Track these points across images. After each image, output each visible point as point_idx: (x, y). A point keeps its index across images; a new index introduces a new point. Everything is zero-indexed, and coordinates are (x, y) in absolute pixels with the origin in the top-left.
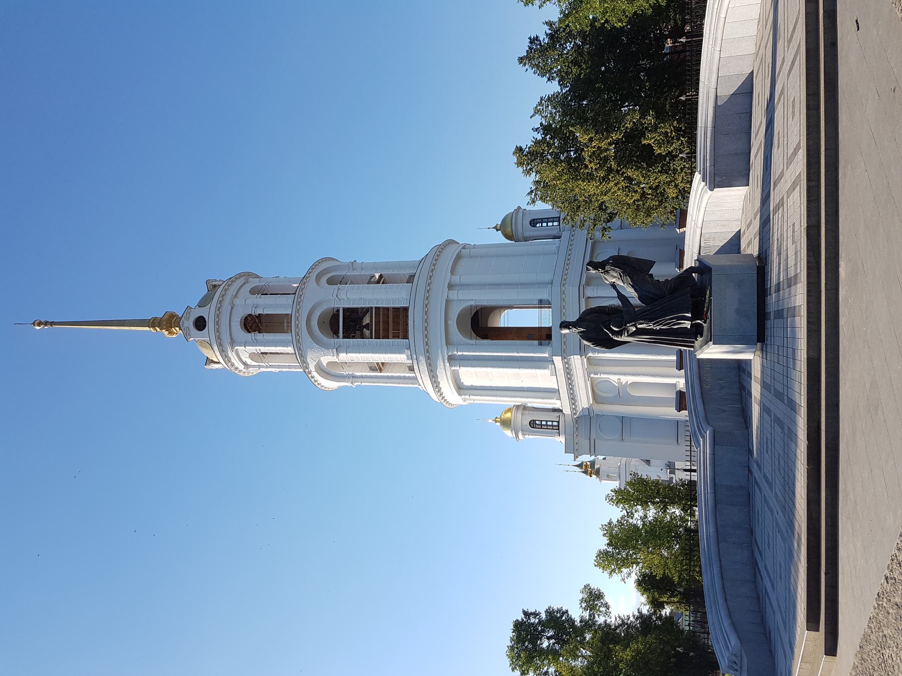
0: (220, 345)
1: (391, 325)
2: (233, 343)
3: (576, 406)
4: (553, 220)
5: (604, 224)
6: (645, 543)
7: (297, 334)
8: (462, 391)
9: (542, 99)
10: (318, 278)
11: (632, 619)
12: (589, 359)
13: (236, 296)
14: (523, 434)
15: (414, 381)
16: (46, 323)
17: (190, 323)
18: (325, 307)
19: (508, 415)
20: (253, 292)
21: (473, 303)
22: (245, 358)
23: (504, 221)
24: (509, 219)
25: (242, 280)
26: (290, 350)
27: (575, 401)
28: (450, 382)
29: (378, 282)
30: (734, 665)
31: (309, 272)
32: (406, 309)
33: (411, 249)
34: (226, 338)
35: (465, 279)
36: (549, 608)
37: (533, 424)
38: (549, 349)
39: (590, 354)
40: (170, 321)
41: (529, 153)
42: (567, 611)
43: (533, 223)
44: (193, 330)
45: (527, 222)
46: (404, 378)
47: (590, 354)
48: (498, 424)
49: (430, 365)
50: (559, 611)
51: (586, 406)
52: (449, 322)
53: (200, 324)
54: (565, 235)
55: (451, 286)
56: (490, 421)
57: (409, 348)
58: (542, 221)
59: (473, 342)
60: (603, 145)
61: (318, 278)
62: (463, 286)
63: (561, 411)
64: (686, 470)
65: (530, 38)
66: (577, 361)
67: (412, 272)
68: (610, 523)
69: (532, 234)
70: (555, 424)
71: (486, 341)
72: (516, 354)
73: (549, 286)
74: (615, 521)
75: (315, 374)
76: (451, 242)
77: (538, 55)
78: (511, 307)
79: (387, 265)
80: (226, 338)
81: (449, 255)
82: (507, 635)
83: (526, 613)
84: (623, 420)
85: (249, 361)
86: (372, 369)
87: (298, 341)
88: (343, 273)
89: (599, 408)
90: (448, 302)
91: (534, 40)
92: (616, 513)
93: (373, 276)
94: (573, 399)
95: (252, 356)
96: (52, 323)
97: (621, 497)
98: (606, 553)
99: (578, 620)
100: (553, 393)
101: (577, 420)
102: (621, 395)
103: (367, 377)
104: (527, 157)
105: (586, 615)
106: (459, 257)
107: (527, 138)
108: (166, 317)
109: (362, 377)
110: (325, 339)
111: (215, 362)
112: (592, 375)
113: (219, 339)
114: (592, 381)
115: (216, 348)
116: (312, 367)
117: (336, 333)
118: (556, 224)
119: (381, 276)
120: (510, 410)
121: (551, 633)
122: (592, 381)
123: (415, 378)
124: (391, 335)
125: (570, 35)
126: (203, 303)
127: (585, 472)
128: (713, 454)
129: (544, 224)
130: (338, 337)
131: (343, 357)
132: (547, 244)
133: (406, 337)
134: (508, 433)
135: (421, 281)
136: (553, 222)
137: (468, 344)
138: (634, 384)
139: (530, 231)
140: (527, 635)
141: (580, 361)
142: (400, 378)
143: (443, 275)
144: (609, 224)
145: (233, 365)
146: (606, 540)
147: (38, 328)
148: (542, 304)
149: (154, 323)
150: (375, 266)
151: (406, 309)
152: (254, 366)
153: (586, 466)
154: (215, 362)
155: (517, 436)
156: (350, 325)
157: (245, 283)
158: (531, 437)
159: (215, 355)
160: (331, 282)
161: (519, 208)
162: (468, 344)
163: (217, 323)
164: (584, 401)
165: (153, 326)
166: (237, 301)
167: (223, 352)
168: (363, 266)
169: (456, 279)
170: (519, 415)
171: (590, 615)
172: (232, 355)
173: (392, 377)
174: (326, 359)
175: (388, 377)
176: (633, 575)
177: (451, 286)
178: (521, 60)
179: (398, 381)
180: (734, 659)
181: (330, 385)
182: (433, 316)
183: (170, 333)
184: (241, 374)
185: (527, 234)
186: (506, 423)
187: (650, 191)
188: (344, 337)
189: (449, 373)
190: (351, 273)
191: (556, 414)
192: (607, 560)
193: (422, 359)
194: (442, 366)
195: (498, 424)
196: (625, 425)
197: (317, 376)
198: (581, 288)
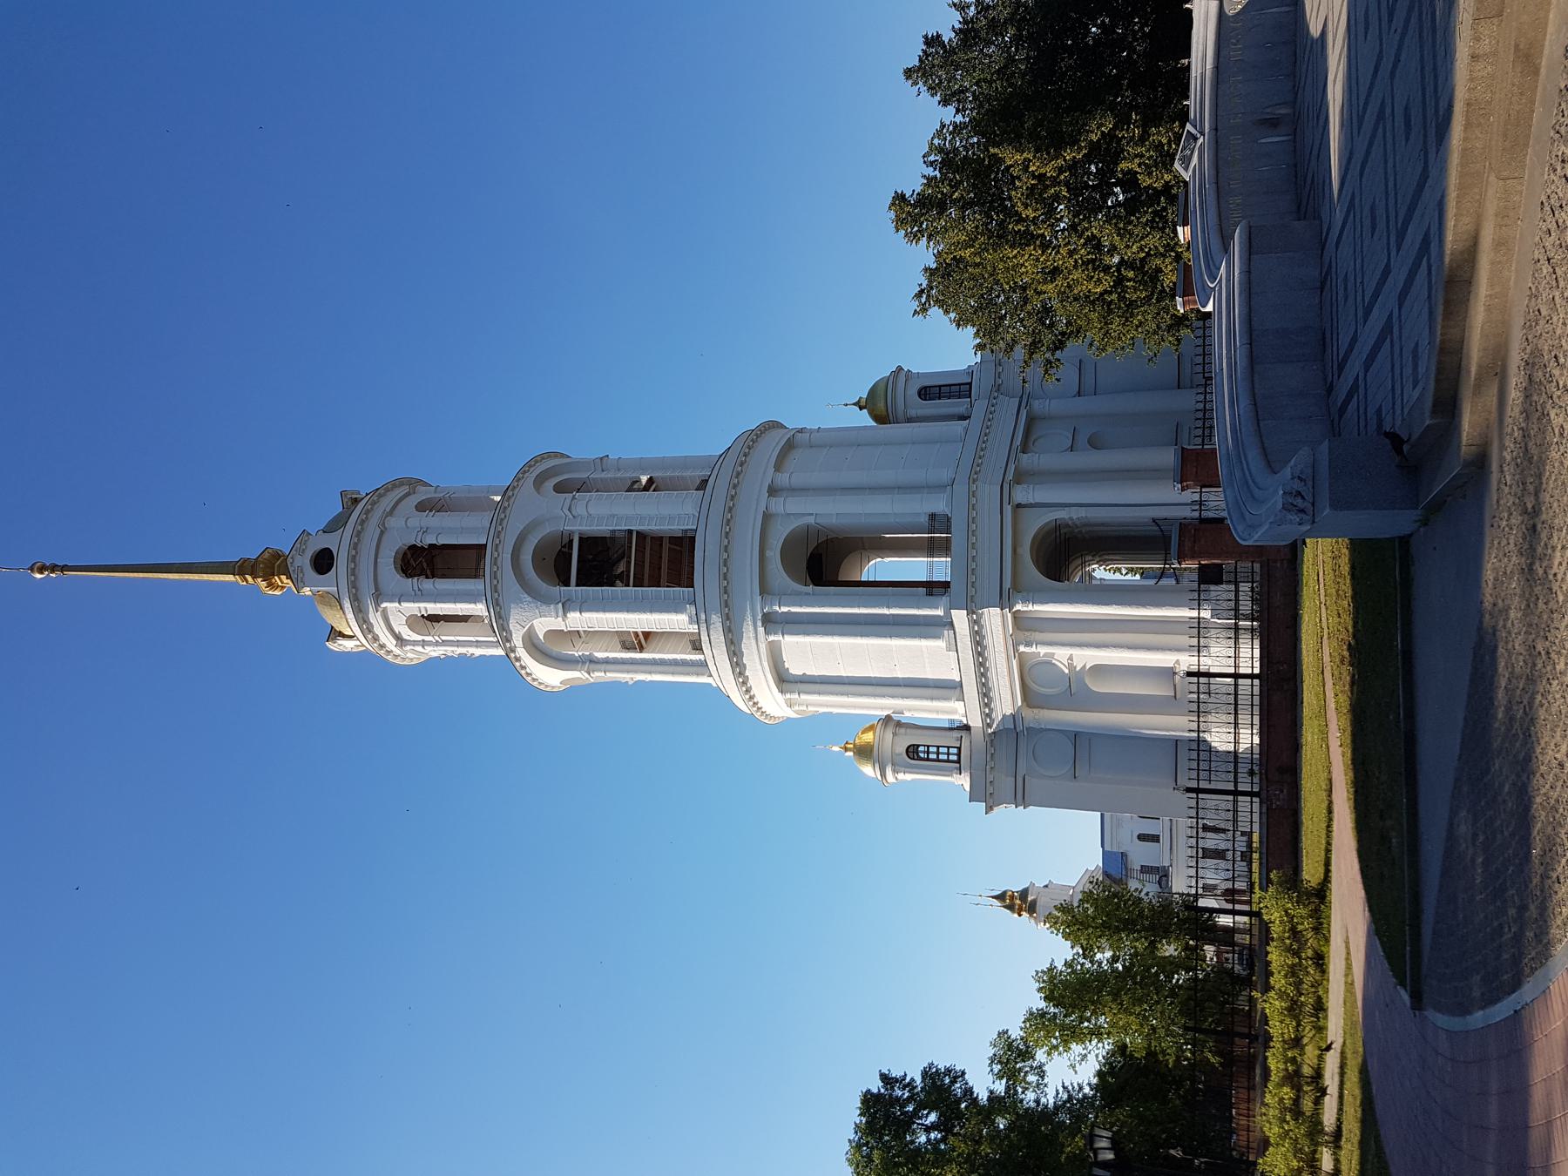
0: (357, 601)
1: (660, 564)
2: (379, 597)
3: (991, 710)
5: (1048, 355)
6: (1116, 995)
7: (494, 576)
8: (786, 686)
9: (943, 126)
10: (539, 482)
11: (1087, 1090)
12: (1017, 616)
13: (391, 513)
14: (895, 771)
15: (700, 669)
16: (53, 568)
17: (304, 561)
19: (869, 737)
20: (421, 507)
21: (811, 520)
22: (397, 631)
23: (872, 392)
24: (882, 386)
25: (405, 489)
26: (479, 609)
27: (991, 700)
28: (766, 664)
29: (646, 489)
30: (1299, 502)
33: (709, 438)
34: (367, 587)
35: (798, 479)
36: (931, 1065)
37: (912, 751)
38: (945, 599)
39: (1018, 607)
40: (271, 565)
42: (963, 1073)
43: (926, 393)
44: (310, 573)
46: (684, 663)
47: (1018, 607)
48: (850, 754)
49: (730, 631)
50: (948, 1071)
51: (1009, 711)
52: (769, 553)
53: (323, 562)
55: (773, 491)
56: (836, 749)
57: (694, 602)
60: (1049, 170)
61: (539, 482)
62: (793, 490)
64: (1189, 790)
65: (926, 37)
66: (994, 618)
68: (1051, 969)
72: (885, 611)
74: (1060, 965)
75: (521, 652)
76: (774, 425)
77: (937, 65)
79: (663, 463)
80: (367, 587)
82: (850, 1116)
83: (886, 1079)
84: (1078, 739)
85: (407, 634)
86: (626, 647)
87: (495, 589)
88: (584, 475)
89: (1030, 715)
90: (767, 517)
91: (932, 41)
93: (639, 481)
94: (985, 693)
95: (412, 622)
96: (64, 568)
98: (1042, 1014)
99: (983, 1096)
100: (951, 688)
101: (994, 739)
102: (1074, 691)
103: (616, 662)
104: (914, 213)
105: (1000, 1087)
106: (790, 446)
107: (913, 177)
108: (266, 555)
109: (607, 661)
111: (344, 636)
112: (1022, 649)
113: (354, 586)
114: (1022, 658)
115: (347, 605)
116: (517, 640)
119: (651, 481)
120: (871, 728)
121: (933, 1117)
122: (1022, 658)
123: (704, 664)
125: (995, 27)
126: (333, 526)
127: (1011, 907)
128: (1248, 272)
130: (567, 584)
131: (577, 620)
134: (868, 770)
135: (720, 487)
137: (799, 594)
138: (1099, 670)
140: (884, 1113)
141: (999, 619)
142: (675, 663)
143: (761, 470)
144: (1058, 354)
145: (376, 639)
147: (38, 576)
149: (242, 568)
150: (642, 465)
152: (415, 643)
153: (1012, 897)
154: (344, 636)
155: (883, 774)
156: (593, 565)
157: (408, 494)
158: (909, 777)
159: (346, 621)
160: (559, 488)
161: (900, 369)
163: (353, 559)
164: (1007, 702)
165: (242, 573)
166: (392, 522)
167: (363, 621)
168: (619, 465)
169: (783, 479)
170: (889, 735)
171: (1008, 1088)
172: (375, 619)
173: (662, 662)
174: (545, 623)
175: (654, 662)
176: (1091, 1057)
177: (773, 491)
178: (908, 73)
179: (671, 669)
180: (1297, 485)
181: (550, 677)
182: (737, 548)
183: (271, 585)
184: (389, 658)
185: (912, 413)
186: (864, 752)
187: (1131, 274)
189: (763, 647)
190: (598, 475)
191: (956, 734)
193: (716, 619)
194: (752, 634)
195: (850, 754)
196: (1082, 748)
197: (527, 660)
198: (1006, 487)
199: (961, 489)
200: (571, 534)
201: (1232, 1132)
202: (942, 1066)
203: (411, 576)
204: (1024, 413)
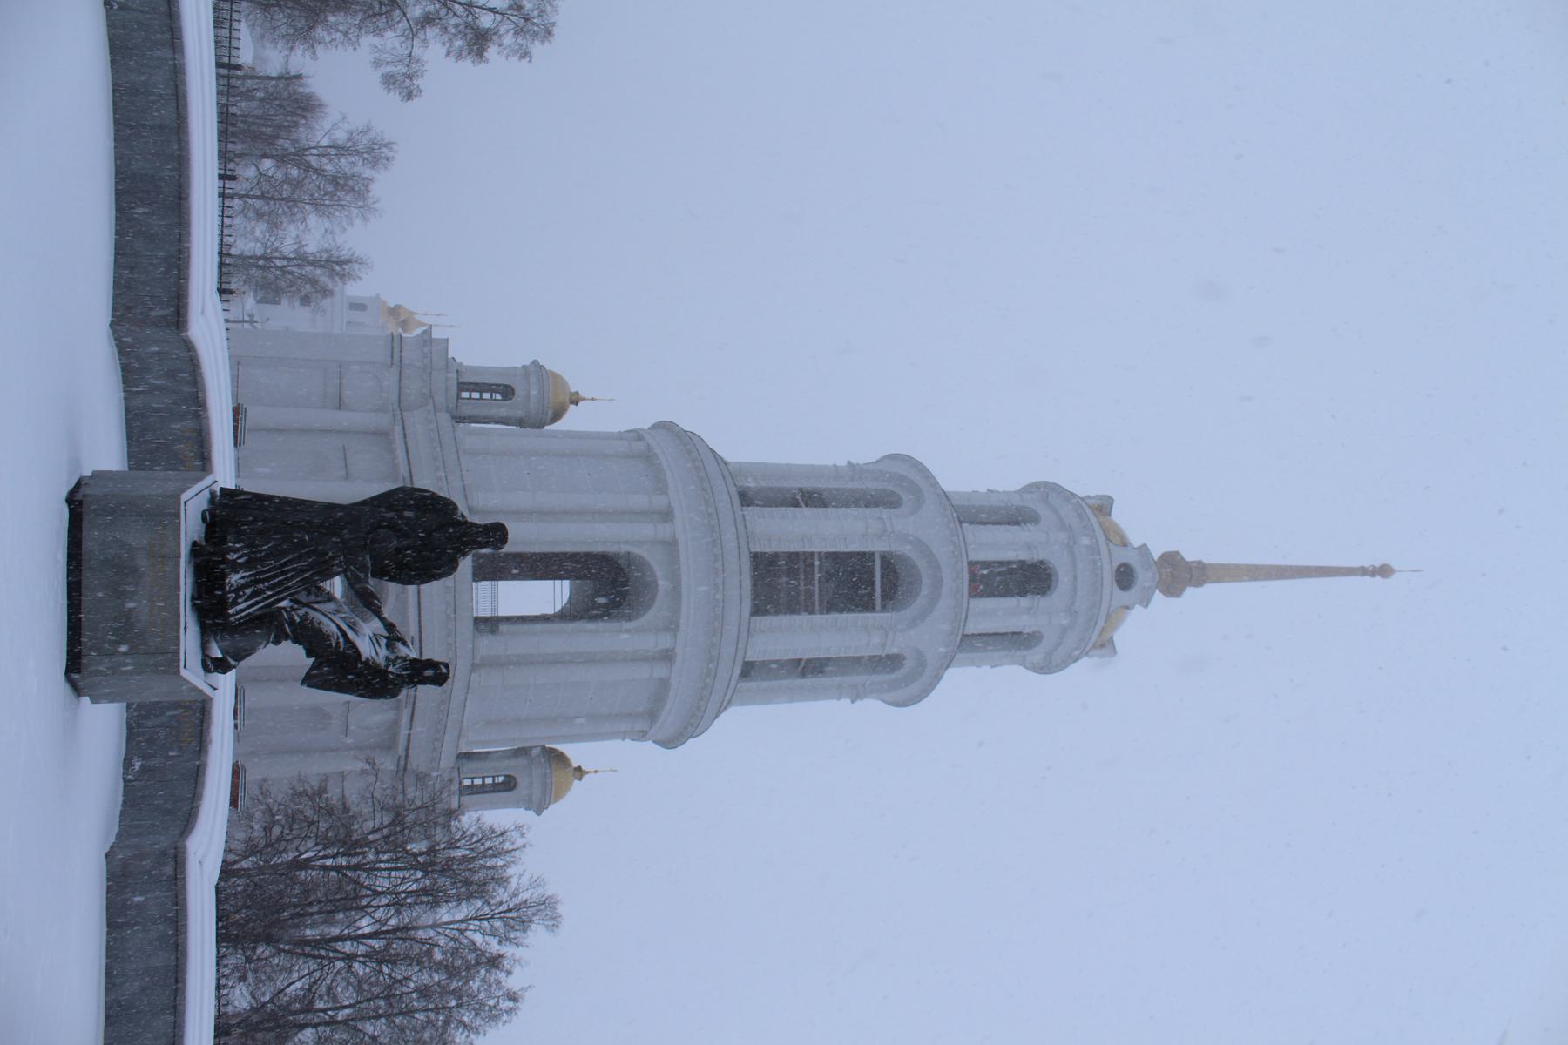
4: (473, 790)
17: (1144, 578)
18: (907, 613)
21: (627, 625)
31: (937, 678)
32: (757, 611)
41: (427, 838)
43: (509, 784)
45: (522, 781)
54: (447, 760)
55: (667, 656)
58: (495, 788)
59: (624, 549)
61: (921, 664)
63: (453, 417)
67: (746, 685)
69: (513, 762)
70: (465, 395)
71: (599, 549)
73: (478, 661)
74: (358, 222)
76: (670, 742)
78: (544, 619)
81: (670, 716)
83: (525, 55)
88: (876, 678)
90: (672, 626)
92: (353, 236)
97: (337, 265)
106: (652, 716)
110: (921, 564)
117: (888, 562)
118: (467, 782)
124: (878, 607)
129: (489, 781)
132: (484, 744)
133: (755, 557)
136: (472, 786)
139: (514, 767)
146: (376, 190)
148: (489, 624)
151: (757, 611)
161: (539, 813)
162: (627, 542)
169: (660, 671)
177: (667, 656)
182: (700, 586)
185: (522, 761)
188: (868, 556)
192: (375, 152)
200: (884, 608)
201: (386, 672)
202: (560, 909)
204: (401, 752)
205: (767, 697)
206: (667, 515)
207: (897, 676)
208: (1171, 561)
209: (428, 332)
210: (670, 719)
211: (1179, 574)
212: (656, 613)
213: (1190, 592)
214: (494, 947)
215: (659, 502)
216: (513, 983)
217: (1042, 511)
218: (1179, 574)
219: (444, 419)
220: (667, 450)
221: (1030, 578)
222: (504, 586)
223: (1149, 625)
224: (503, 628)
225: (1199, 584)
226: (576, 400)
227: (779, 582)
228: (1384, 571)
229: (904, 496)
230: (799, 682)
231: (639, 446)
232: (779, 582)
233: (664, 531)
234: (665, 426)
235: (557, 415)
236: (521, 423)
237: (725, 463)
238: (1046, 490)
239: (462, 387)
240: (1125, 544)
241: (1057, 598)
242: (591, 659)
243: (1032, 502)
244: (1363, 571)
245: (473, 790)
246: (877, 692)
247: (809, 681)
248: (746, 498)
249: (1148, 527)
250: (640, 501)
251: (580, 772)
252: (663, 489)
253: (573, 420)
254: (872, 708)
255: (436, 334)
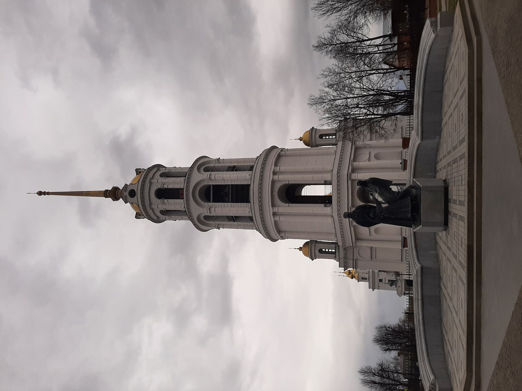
17: (126, 194)
25: (156, 169)
32: (249, 186)
43: (321, 136)
54: (340, 144)
55: (274, 173)
58: (326, 135)
61: (199, 169)
69: (320, 143)
70: (333, 251)
76: (274, 147)
88: (212, 165)
90: (273, 182)
106: (279, 156)
118: (334, 137)
129: (327, 137)
139: (319, 141)
143: (270, 167)
148: (326, 183)
151: (249, 186)
166: (153, 181)
177: (274, 173)
182: (263, 193)
185: (318, 143)
188: (213, 202)
190: (217, 165)
199: (340, 144)
200: (210, 186)
203: (160, 199)
205: (245, 160)
206: (274, 214)
207: (203, 164)
208: (116, 199)
209: (345, 270)
210: (275, 155)
211: (114, 194)
212: (278, 186)
213: (110, 188)
214: (327, 89)
215: (277, 218)
216: (323, 80)
217: (159, 214)
218: (114, 194)
219: (340, 244)
220: (274, 233)
221: (163, 194)
222: (323, 194)
223: (124, 179)
224: (323, 182)
225: (107, 191)
226: (300, 249)
227: (240, 194)
228: (40, 193)
229: (203, 219)
230: (235, 164)
231: (283, 235)
232: (240, 194)
233: (276, 210)
234: (274, 240)
235: (306, 244)
236: (316, 242)
237: (256, 229)
238: (157, 221)
239: (334, 253)
240: (132, 204)
241: (154, 188)
242: (295, 215)
243: (162, 217)
244: (48, 193)
245: (332, 135)
246: (211, 161)
247: (232, 165)
248: (251, 219)
249: (124, 209)
250: (282, 219)
251: (301, 139)
252: (276, 222)
253: (301, 242)
254: (213, 155)
255: (342, 269)
